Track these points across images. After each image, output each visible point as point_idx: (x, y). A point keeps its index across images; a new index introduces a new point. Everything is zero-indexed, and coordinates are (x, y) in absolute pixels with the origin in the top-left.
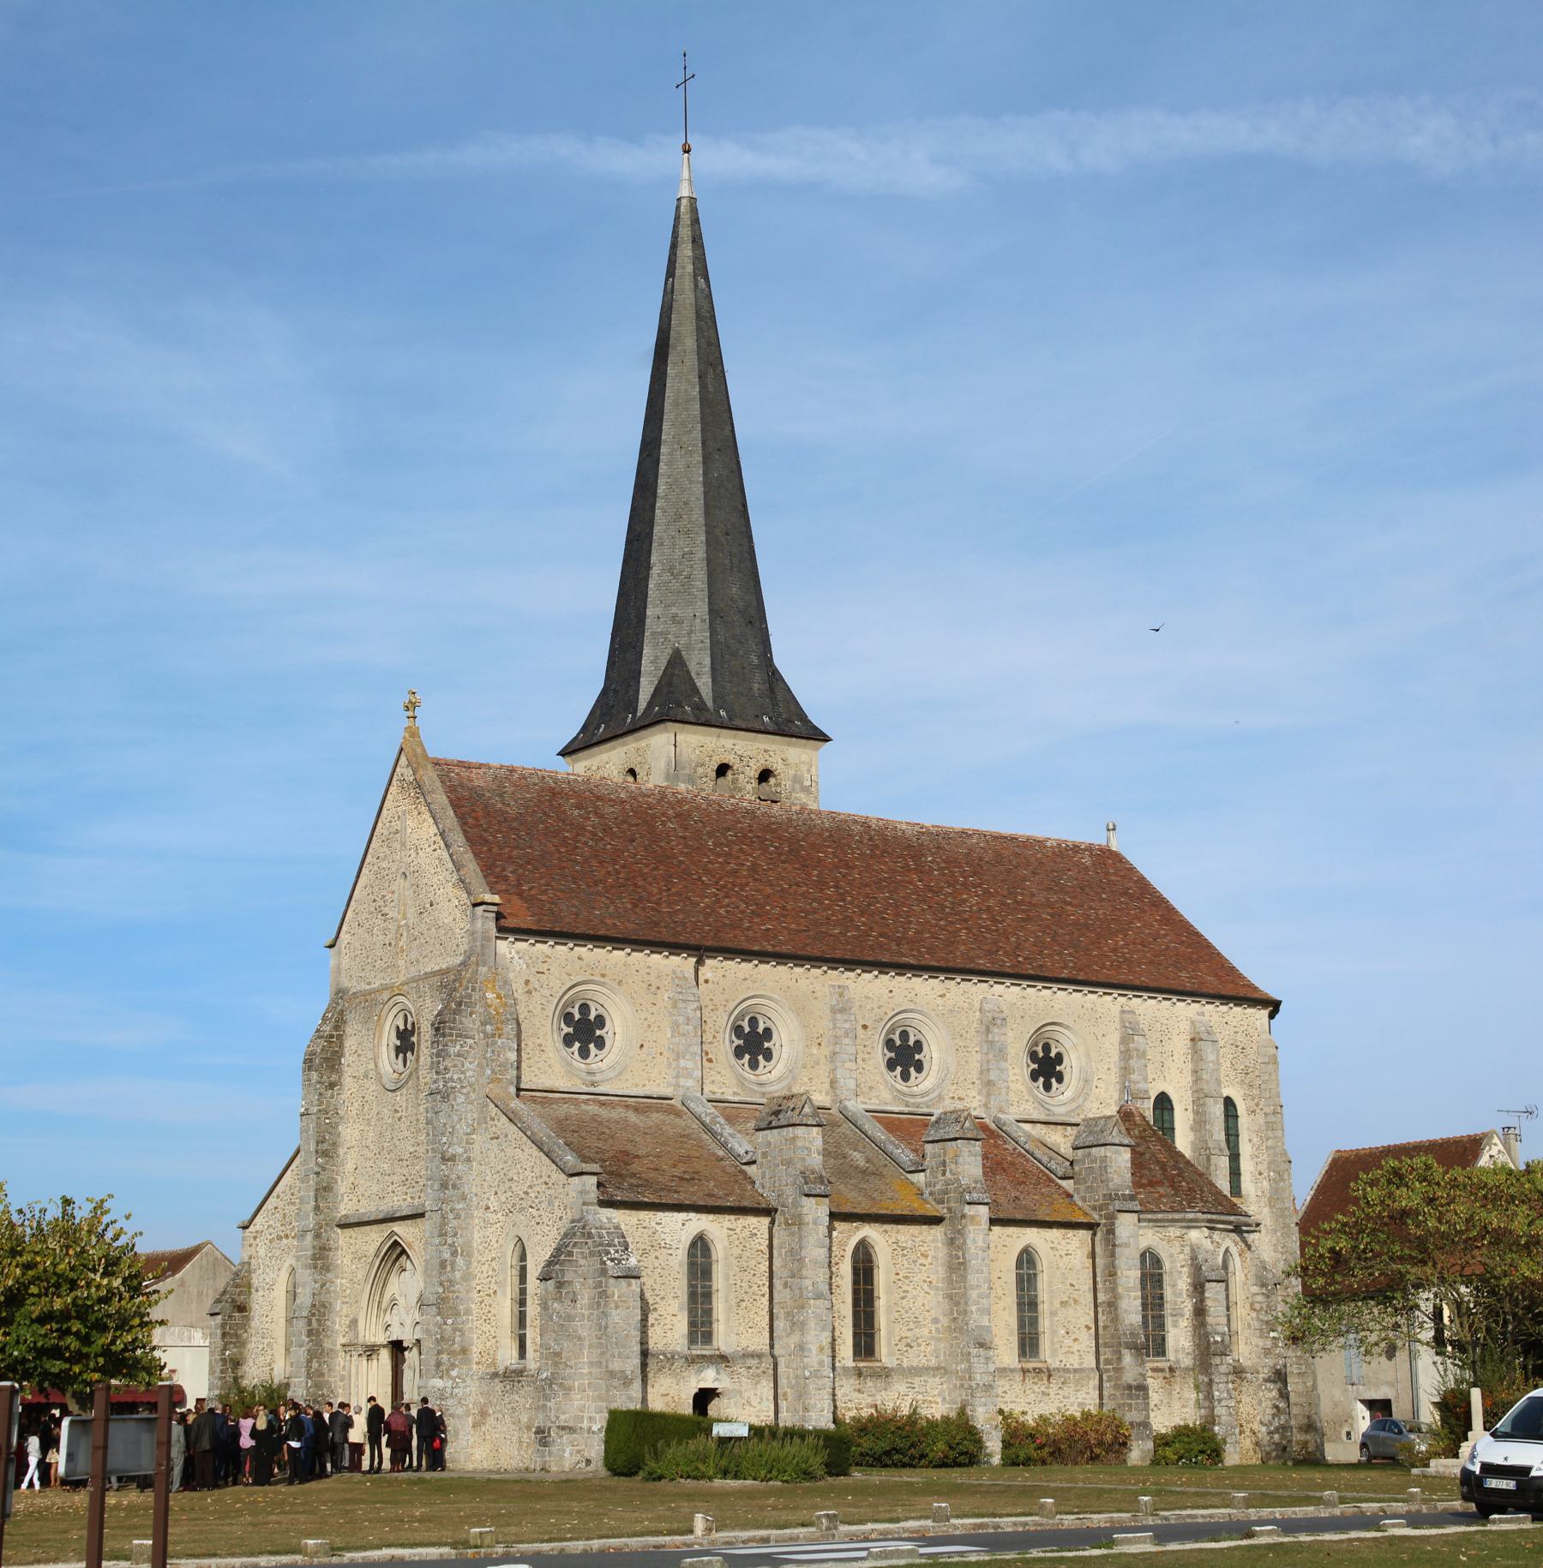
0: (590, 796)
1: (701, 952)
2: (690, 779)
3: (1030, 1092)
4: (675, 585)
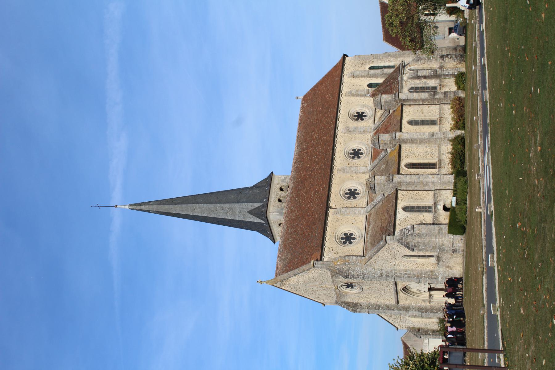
0: (286, 236)
1: (328, 207)
2: (282, 209)
4: (231, 212)
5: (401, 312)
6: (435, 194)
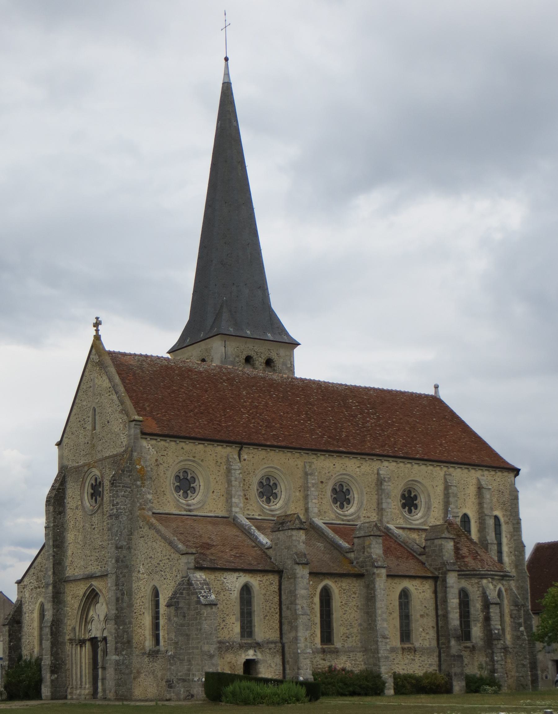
0: (185, 373)
1: (241, 445)
2: (233, 363)
5: (51, 588)
6: (275, 643)
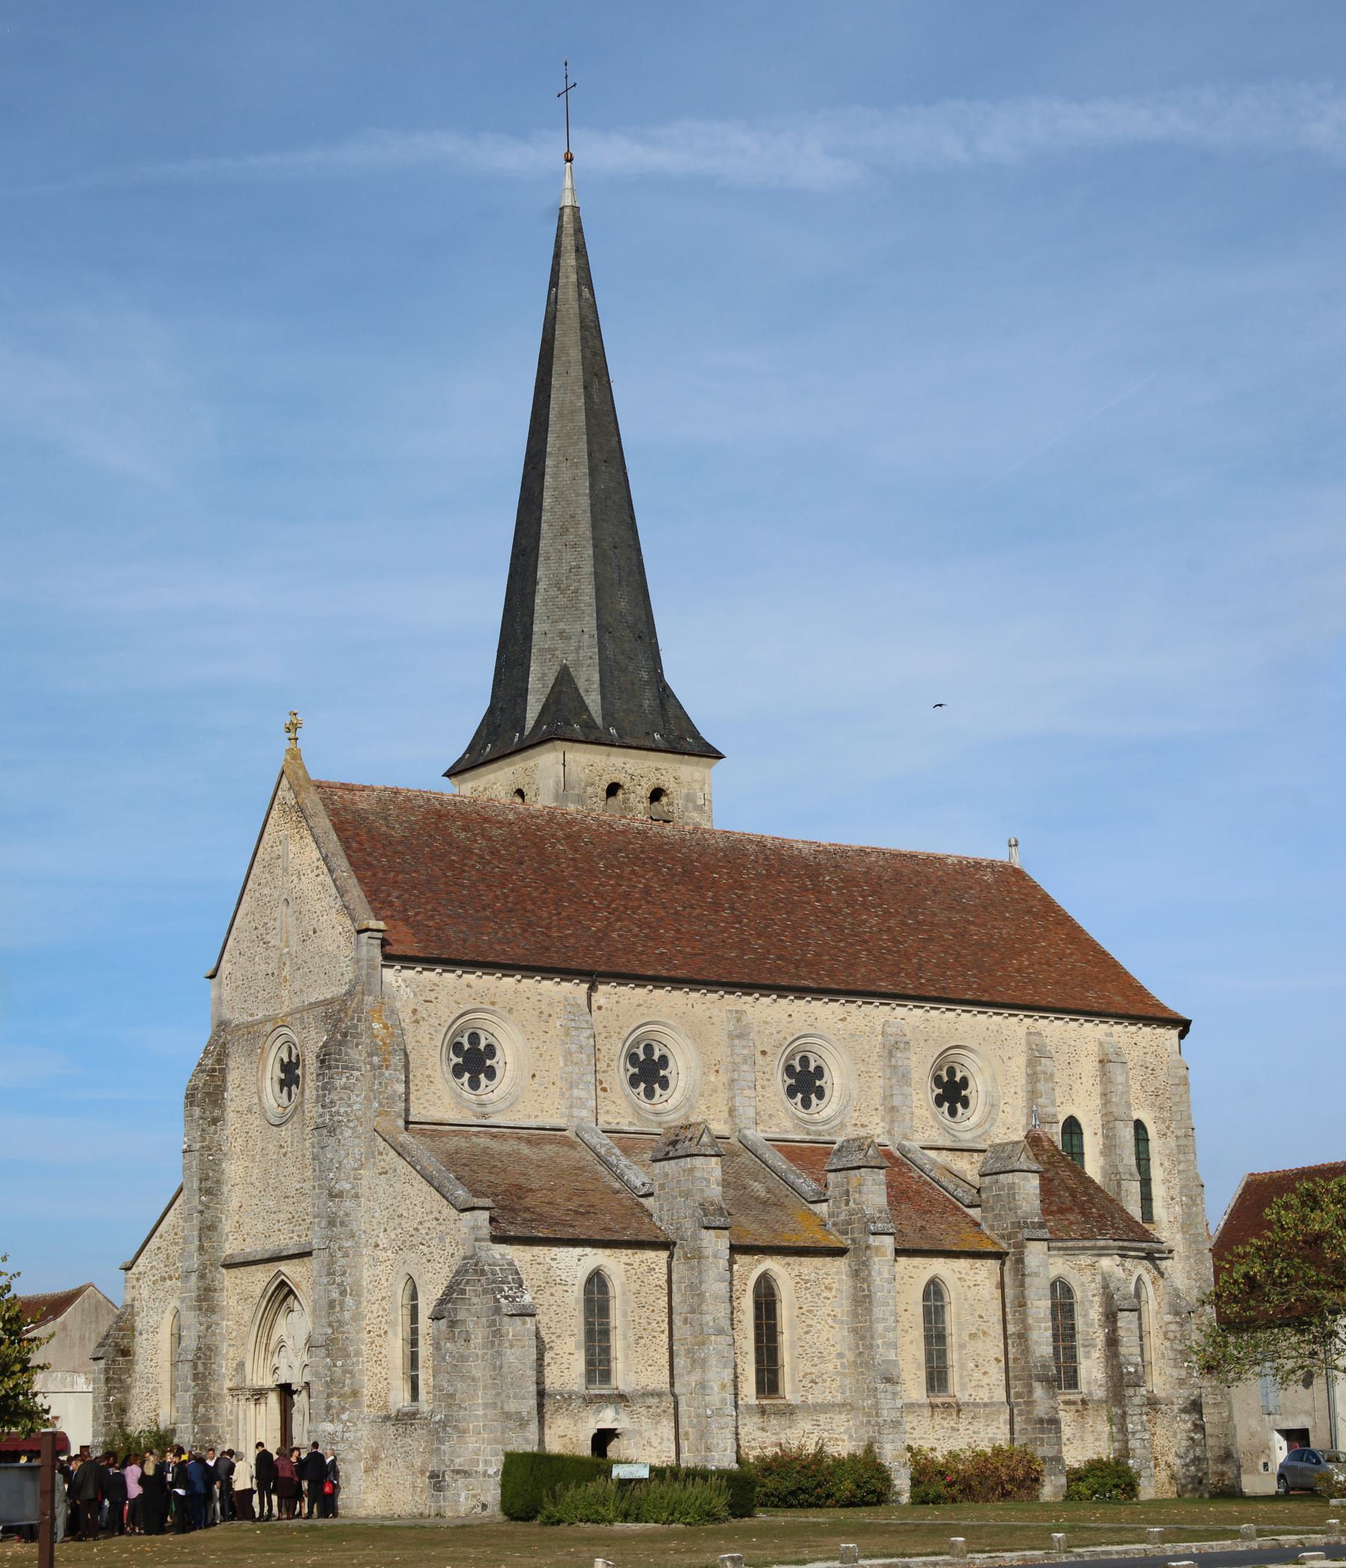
1: (593, 977)
3: (935, 1117)
4: (562, 600)
